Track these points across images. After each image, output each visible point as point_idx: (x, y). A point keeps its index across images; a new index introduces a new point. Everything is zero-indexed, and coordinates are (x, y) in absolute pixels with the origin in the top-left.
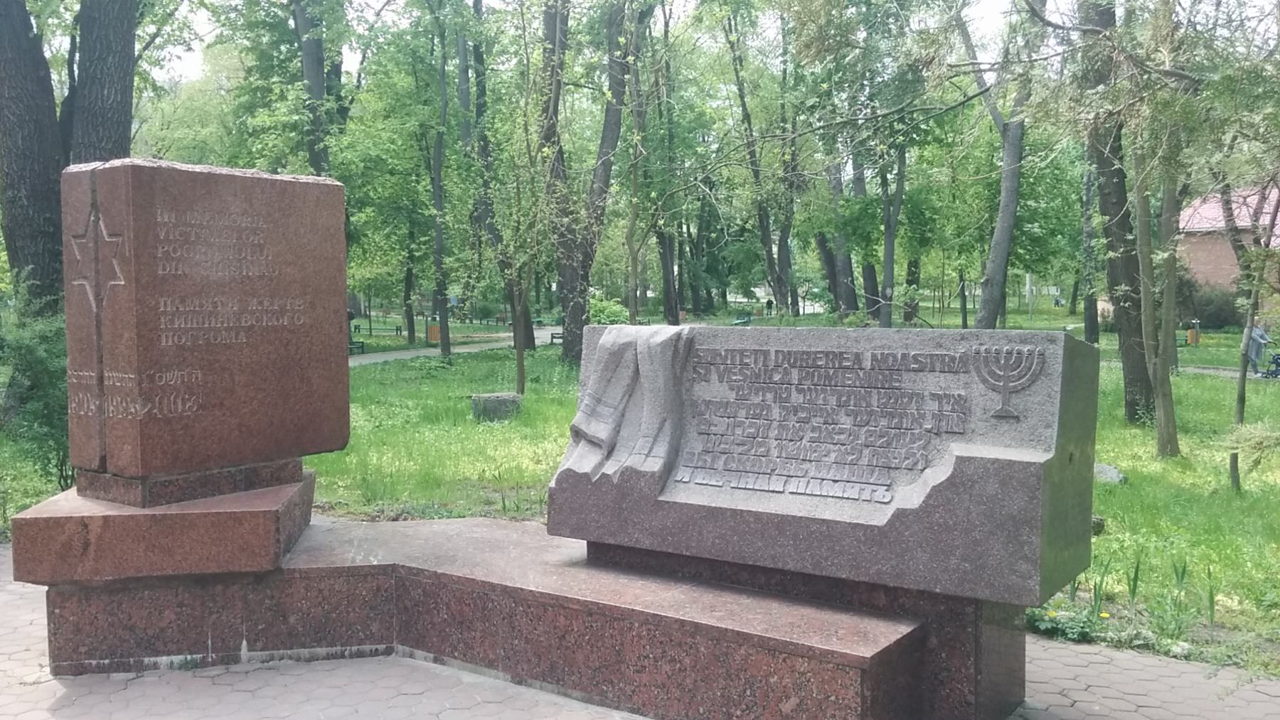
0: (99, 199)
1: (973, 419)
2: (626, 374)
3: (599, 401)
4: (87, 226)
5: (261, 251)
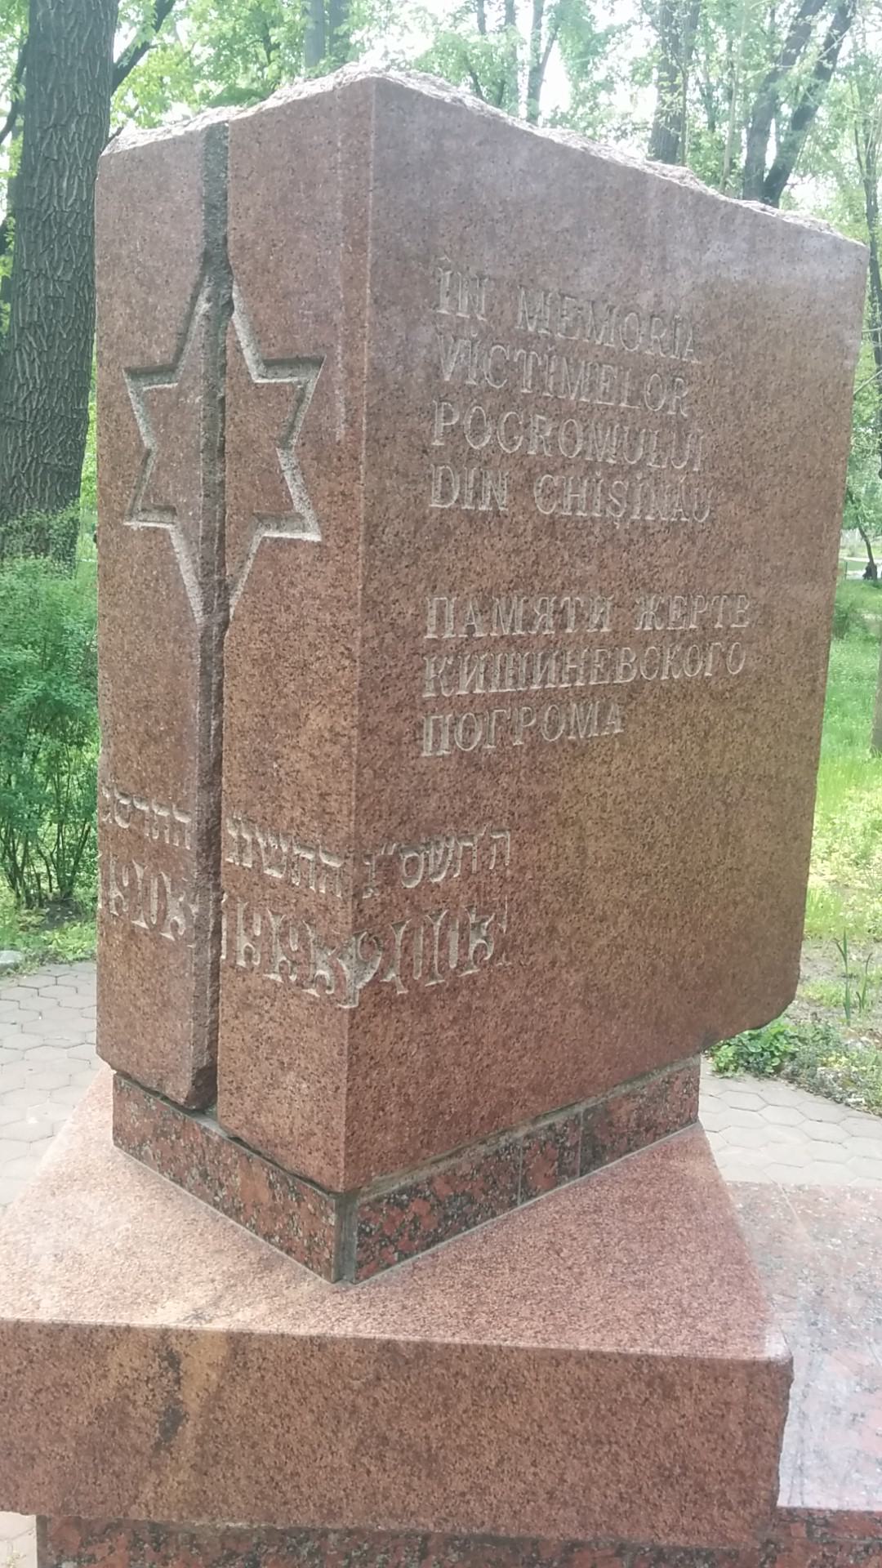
0: (236, 229)
4: (183, 336)
5: (681, 440)
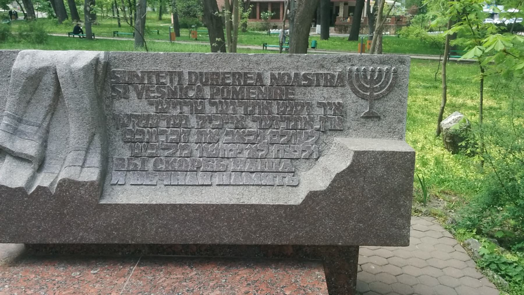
1: (349, 119)
2: (46, 96)
3: (20, 121)
